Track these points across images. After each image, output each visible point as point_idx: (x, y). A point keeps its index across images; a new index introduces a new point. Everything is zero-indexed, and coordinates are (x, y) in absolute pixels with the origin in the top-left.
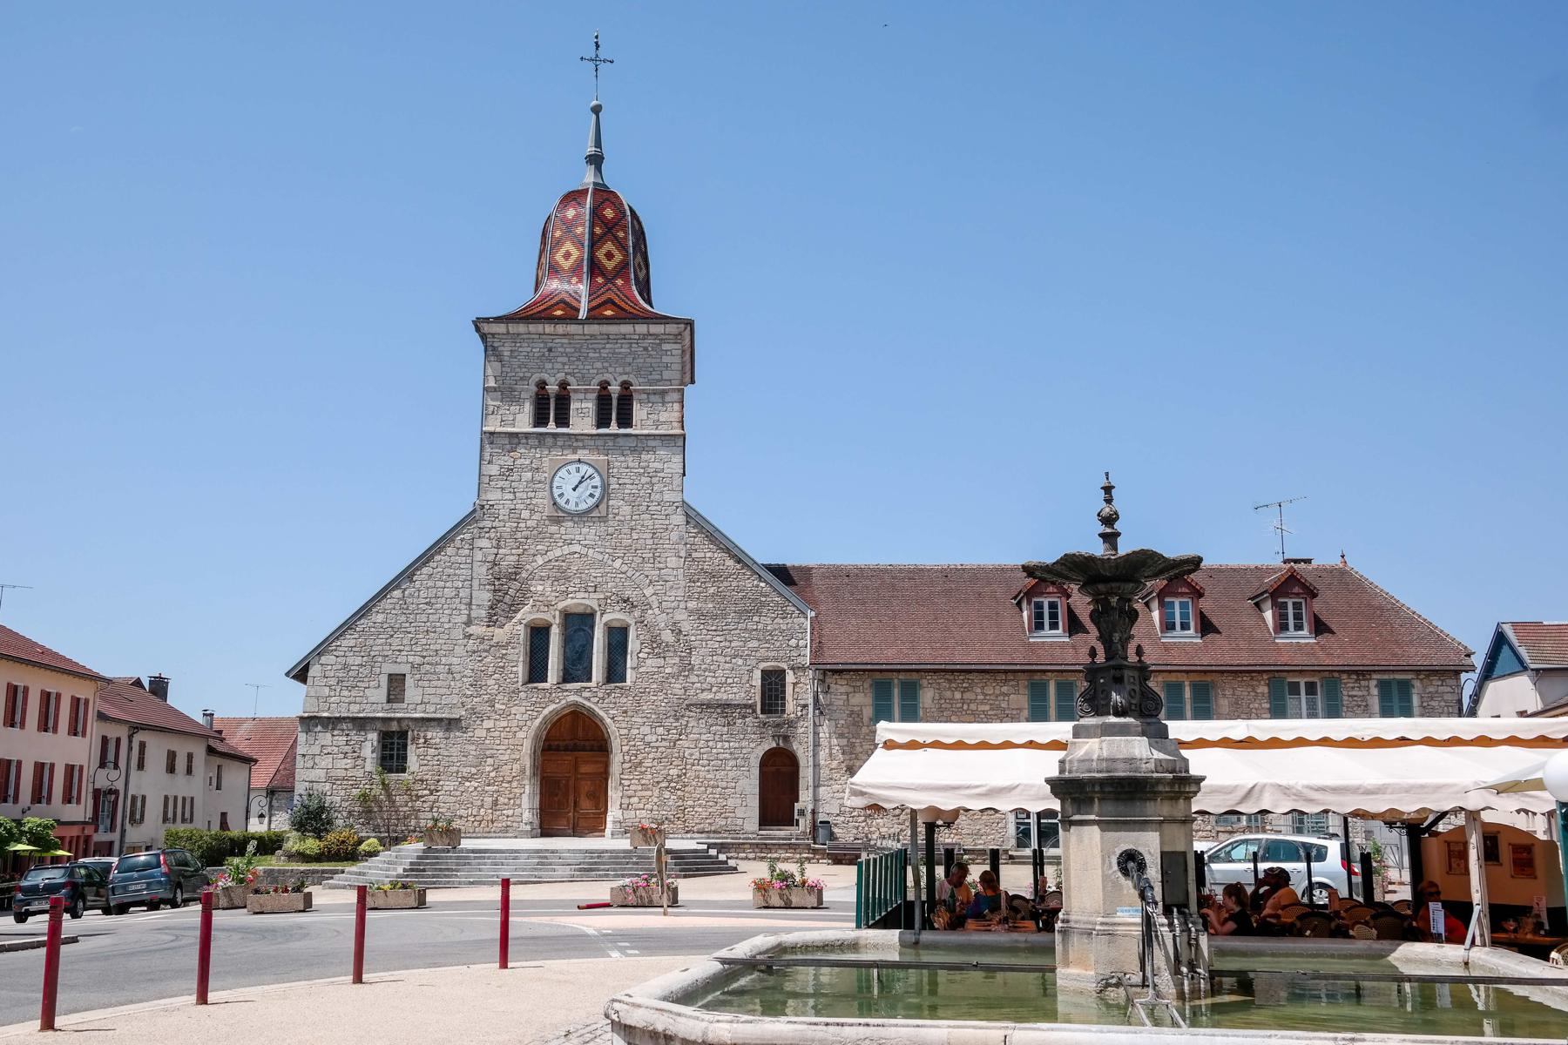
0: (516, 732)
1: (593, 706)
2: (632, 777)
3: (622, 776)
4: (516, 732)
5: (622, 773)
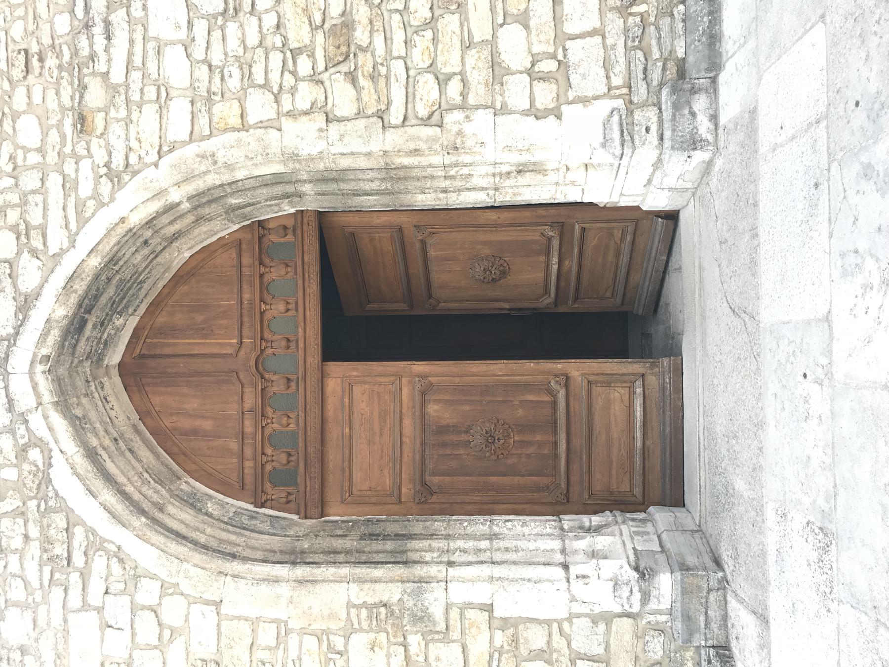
0: (14, 434)
1: (58, 280)
2: (398, 67)
3: (395, 116)
4: (14, 434)
5: (380, 115)
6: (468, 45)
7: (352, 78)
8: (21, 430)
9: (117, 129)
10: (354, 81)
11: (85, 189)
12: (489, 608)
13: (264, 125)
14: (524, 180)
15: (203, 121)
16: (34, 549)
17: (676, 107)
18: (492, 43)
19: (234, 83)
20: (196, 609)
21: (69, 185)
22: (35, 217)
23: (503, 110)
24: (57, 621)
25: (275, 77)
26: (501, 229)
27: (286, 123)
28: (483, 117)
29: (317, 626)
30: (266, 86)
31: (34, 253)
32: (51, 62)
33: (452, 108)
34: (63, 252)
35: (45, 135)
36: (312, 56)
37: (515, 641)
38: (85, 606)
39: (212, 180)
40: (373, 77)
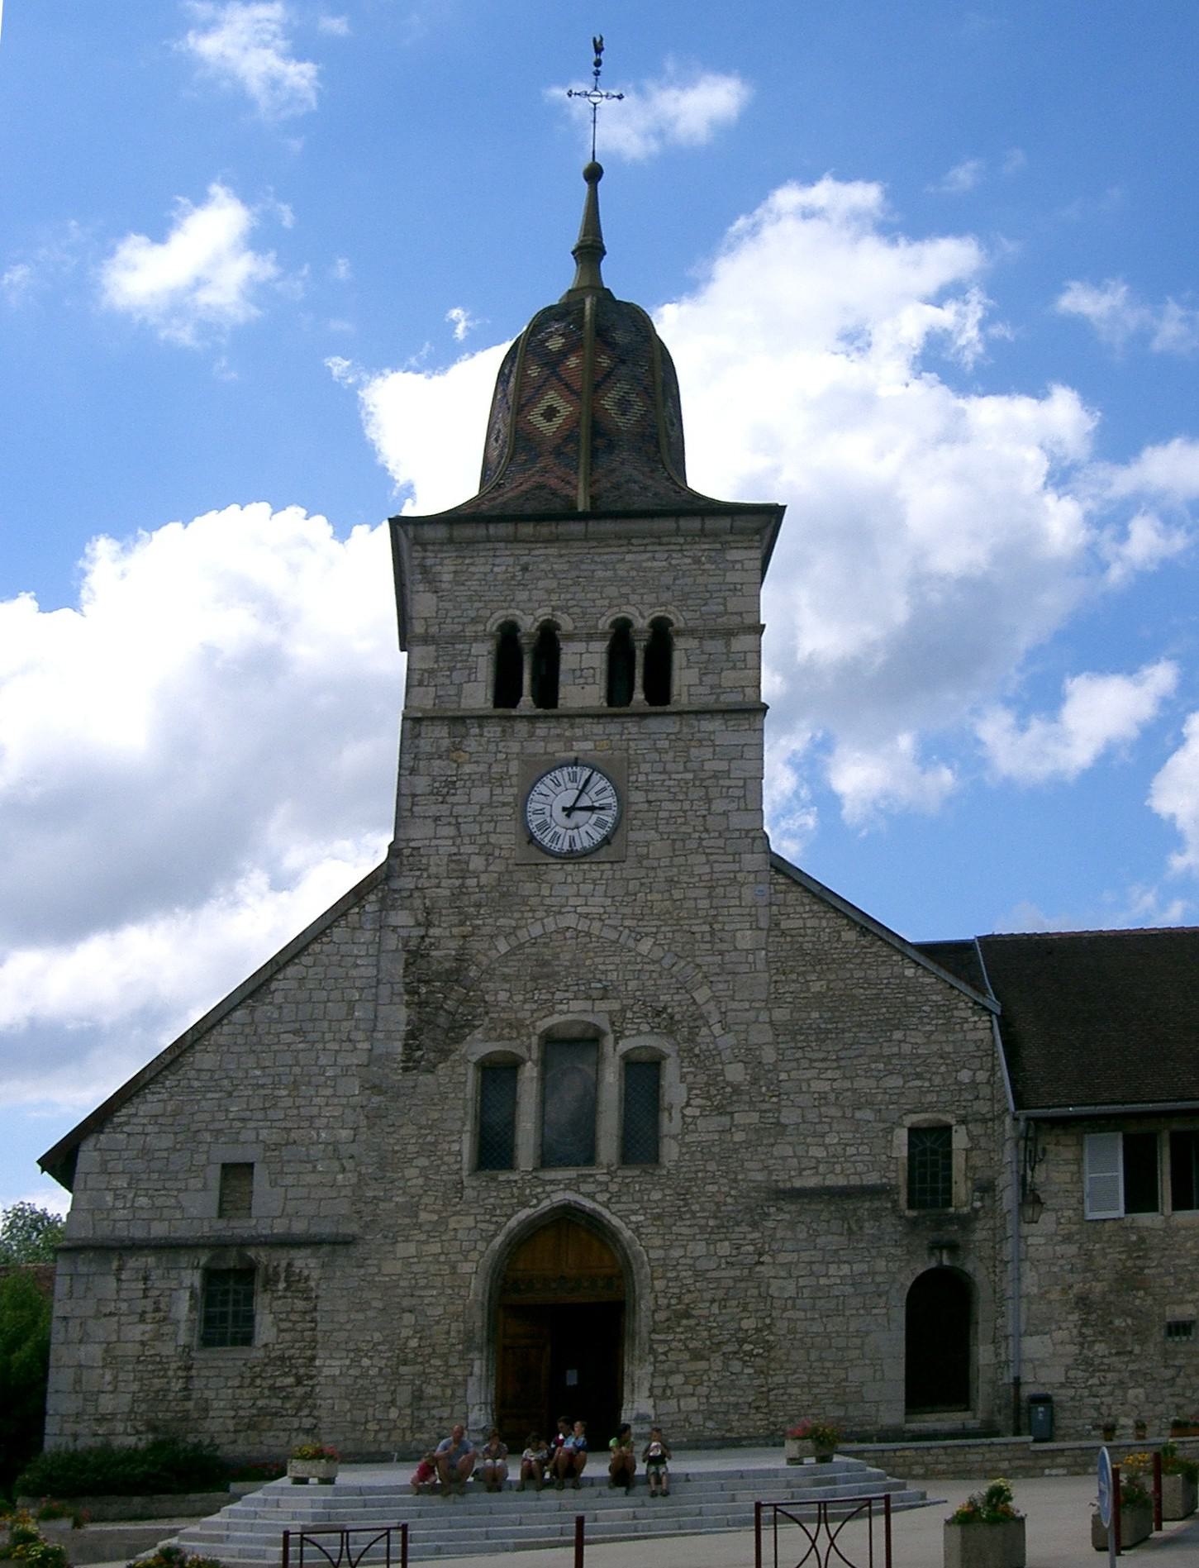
1: (599, 1208)
2: (671, 1337)
3: (655, 1336)
6: (678, 1363)
7: (668, 1320)
8: (544, 1195)
9: (655, 1230)
10: (667, 1320)
11: (633, 1218)
12: (471, 1375)
13: (652, 1288)
15: (656, 1263)
16: (499, 1201)
18: (678, 1372)
19: (670, 1275)
20: (475, 1265)
21: (635, 1213)
22: (624, 1199)
23: (653, 1376)
24: (473, 1211)
26: (1054, 1472)
27: (653, 1295)
30: (668, 1287)
31: (610, 1199)
32: (682, 1203)
33: (655, 1358)
35: (655, 1201)
38: (477, 1222)
39: (634, 1267)
40: (669, 1328)
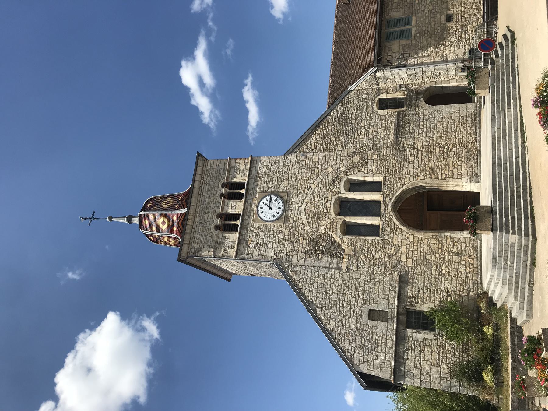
1: (395, 197)
7: (434, 174)
11: (399, 186)
12: (450, 236)
14: (457, 187)
17: (476, 178)
23: (454, 178)
25: (424, 174)
28: (451, 179)
29: (427, 238)
34: (395, 194)
36: (429, 172)
37: (454, 240)
38: (396, 235)
